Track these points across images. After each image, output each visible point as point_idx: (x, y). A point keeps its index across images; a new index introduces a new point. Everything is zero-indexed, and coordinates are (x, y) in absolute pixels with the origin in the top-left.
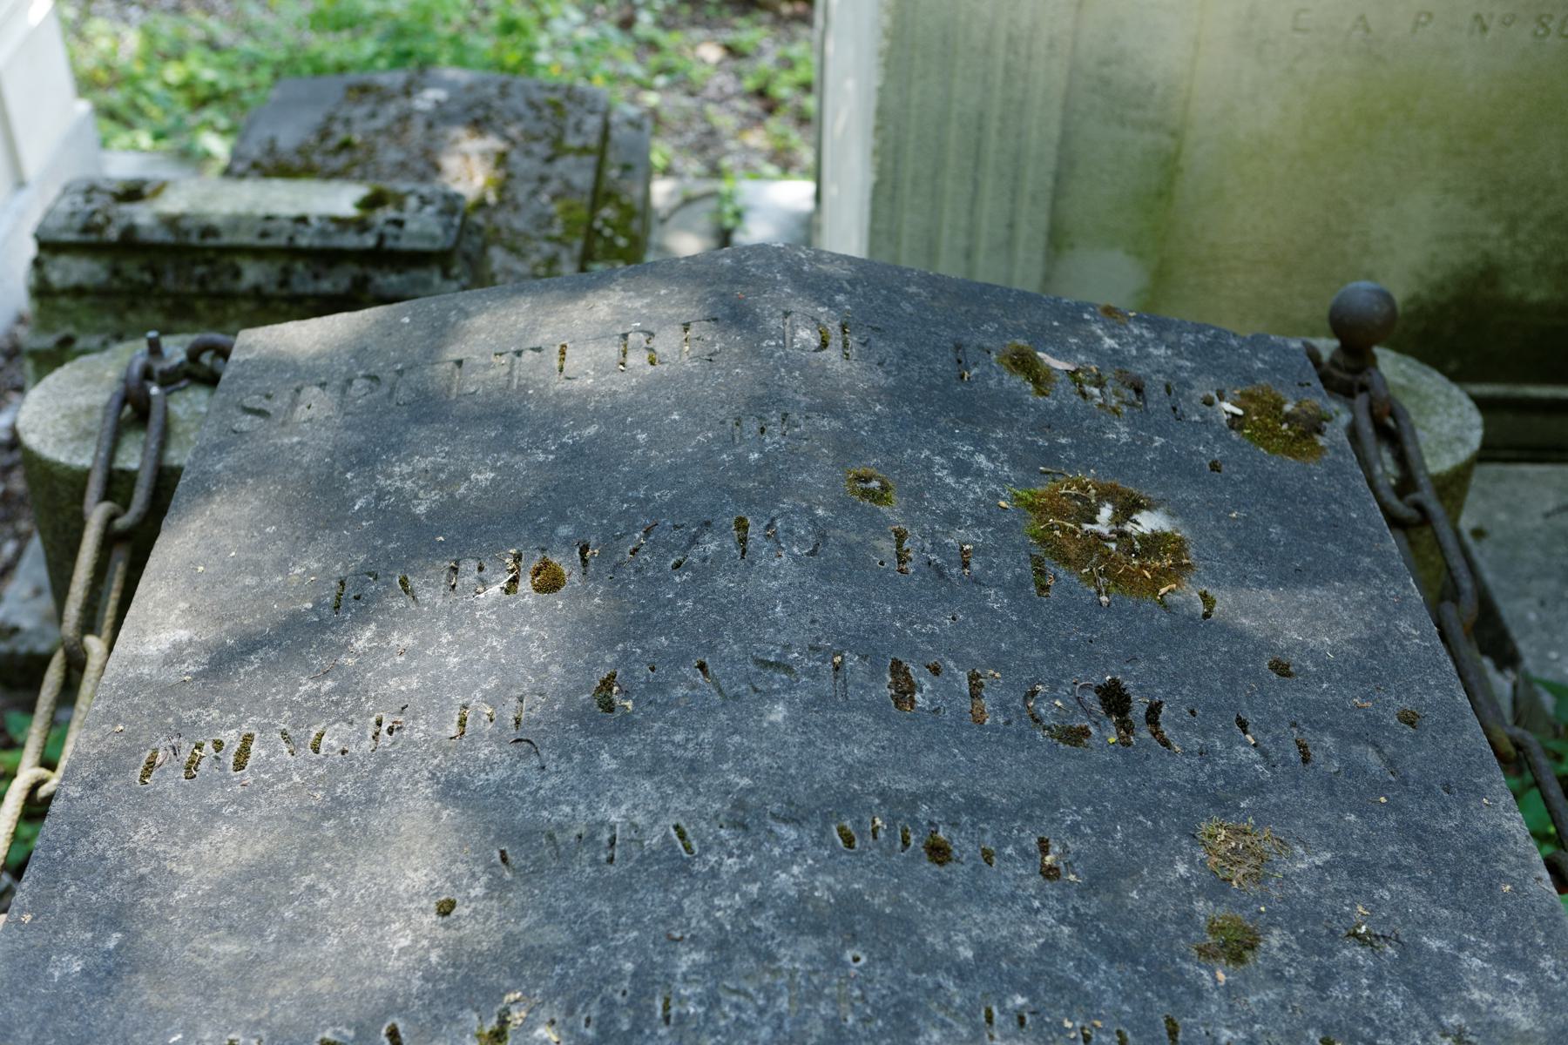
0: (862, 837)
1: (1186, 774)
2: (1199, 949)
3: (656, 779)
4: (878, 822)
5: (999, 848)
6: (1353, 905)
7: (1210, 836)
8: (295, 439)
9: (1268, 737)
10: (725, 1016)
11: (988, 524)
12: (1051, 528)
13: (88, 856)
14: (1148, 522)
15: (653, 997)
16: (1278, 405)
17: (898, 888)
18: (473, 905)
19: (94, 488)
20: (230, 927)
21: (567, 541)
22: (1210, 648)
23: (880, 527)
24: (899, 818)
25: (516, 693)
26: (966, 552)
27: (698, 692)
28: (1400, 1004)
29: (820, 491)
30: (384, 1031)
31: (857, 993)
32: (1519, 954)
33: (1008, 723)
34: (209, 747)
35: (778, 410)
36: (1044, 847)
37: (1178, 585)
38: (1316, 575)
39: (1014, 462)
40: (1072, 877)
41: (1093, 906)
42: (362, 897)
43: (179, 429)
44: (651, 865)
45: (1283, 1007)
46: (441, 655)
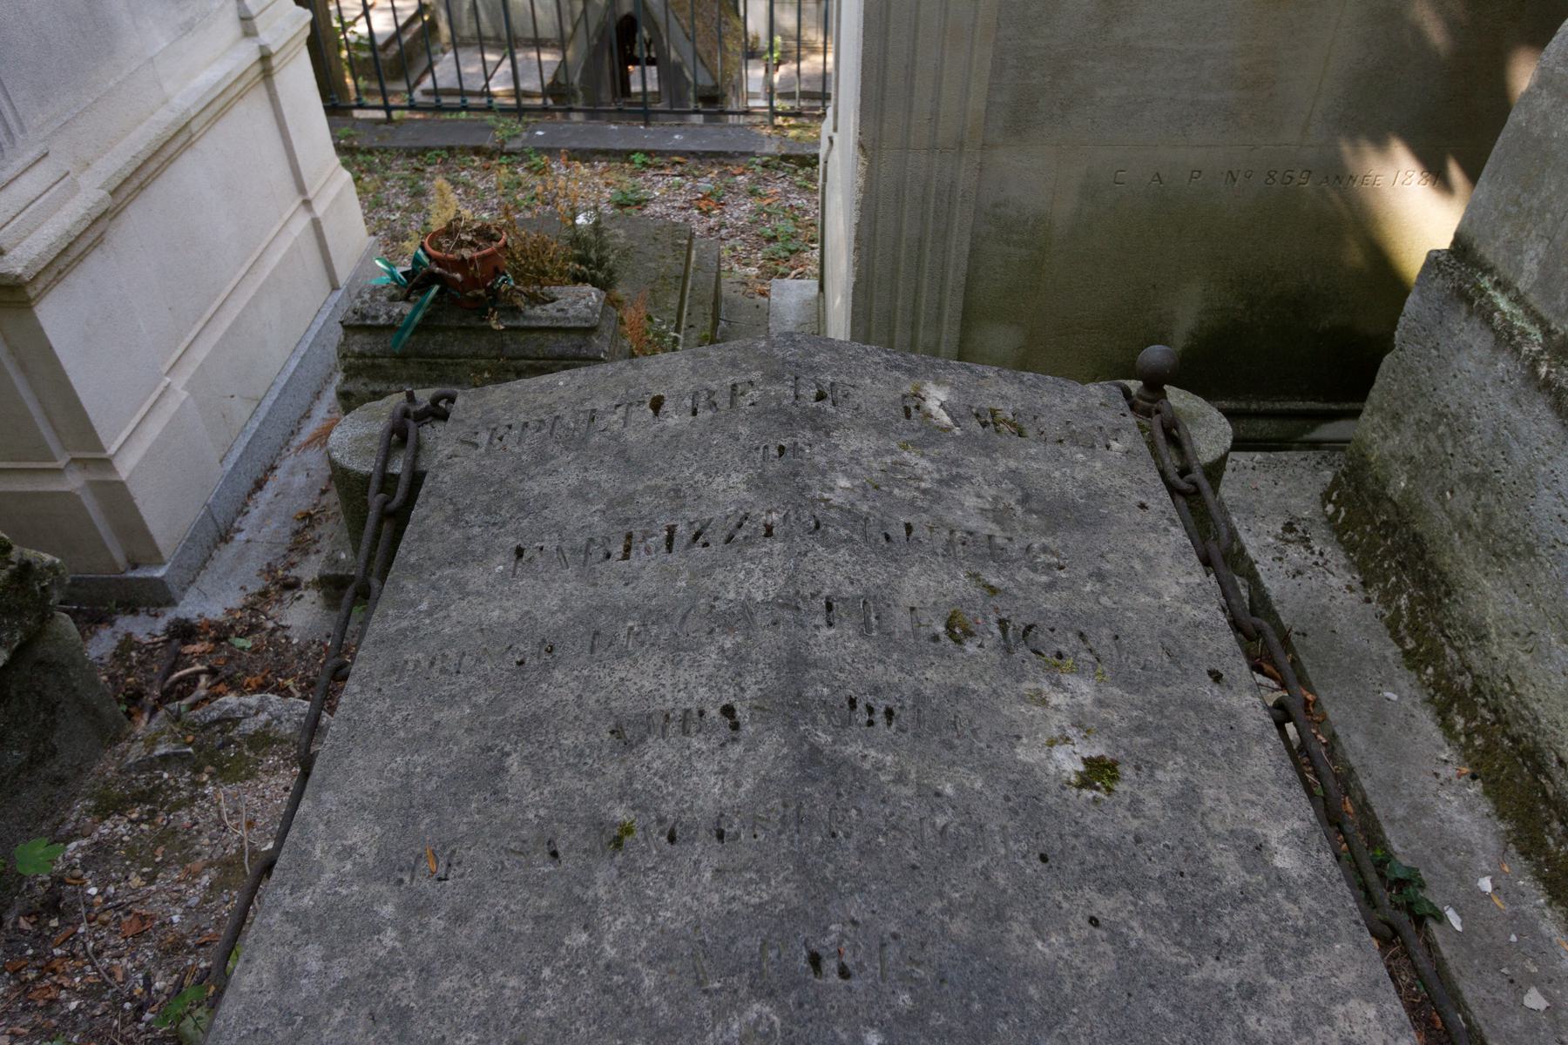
19: (374, 485)
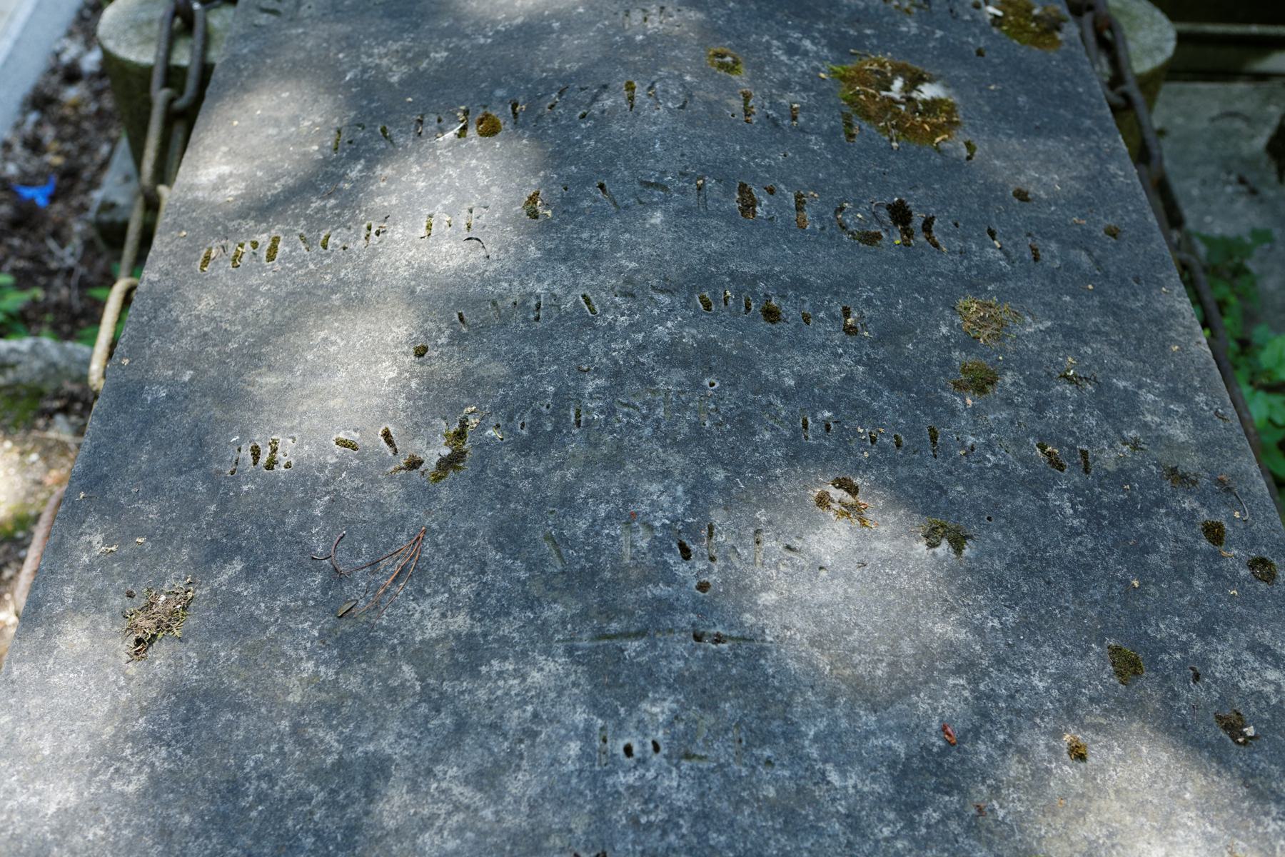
0: (717, 303)
1: (950, 266)
2: (954, 383)
3: (569, 264)
4: (729, 293)
5: (814, 313)
6: (1065, 357)
7: (965, 308)
8: (300, 30)
9: (1010, 243)
10: (620, 421)
11: (811, 90)
12: (857, 93)
13: (166, 320)
14: (928, 91)
15: (568, 409)
16: (1029, 9)
17: (743, 338)
18: (440, 350)
19: (157, 78)
20: (269, 366)
21: (502, 100)
22: (970, 181)
23: (732, 90)
24: (743, 292)
25: (467, 206)
26: (795, 109)
27: (598, 204)
28: (1094, 423)
29: (688, 63)
30: (380, 433)
31: (713, 406)
32: (1181, 392)
33: (823, 229)
34: (248, 246)
35: (657, 4)
36: (846, 312)
37: (950, 136)
38: (1051, 131)
39: (832, 45)
40: (866, 334)
41: (881, 353)
42: (361, 345)
43: (216, 36)
44: (566, 321)
45: (1012, 423)
46: (412, 181)
